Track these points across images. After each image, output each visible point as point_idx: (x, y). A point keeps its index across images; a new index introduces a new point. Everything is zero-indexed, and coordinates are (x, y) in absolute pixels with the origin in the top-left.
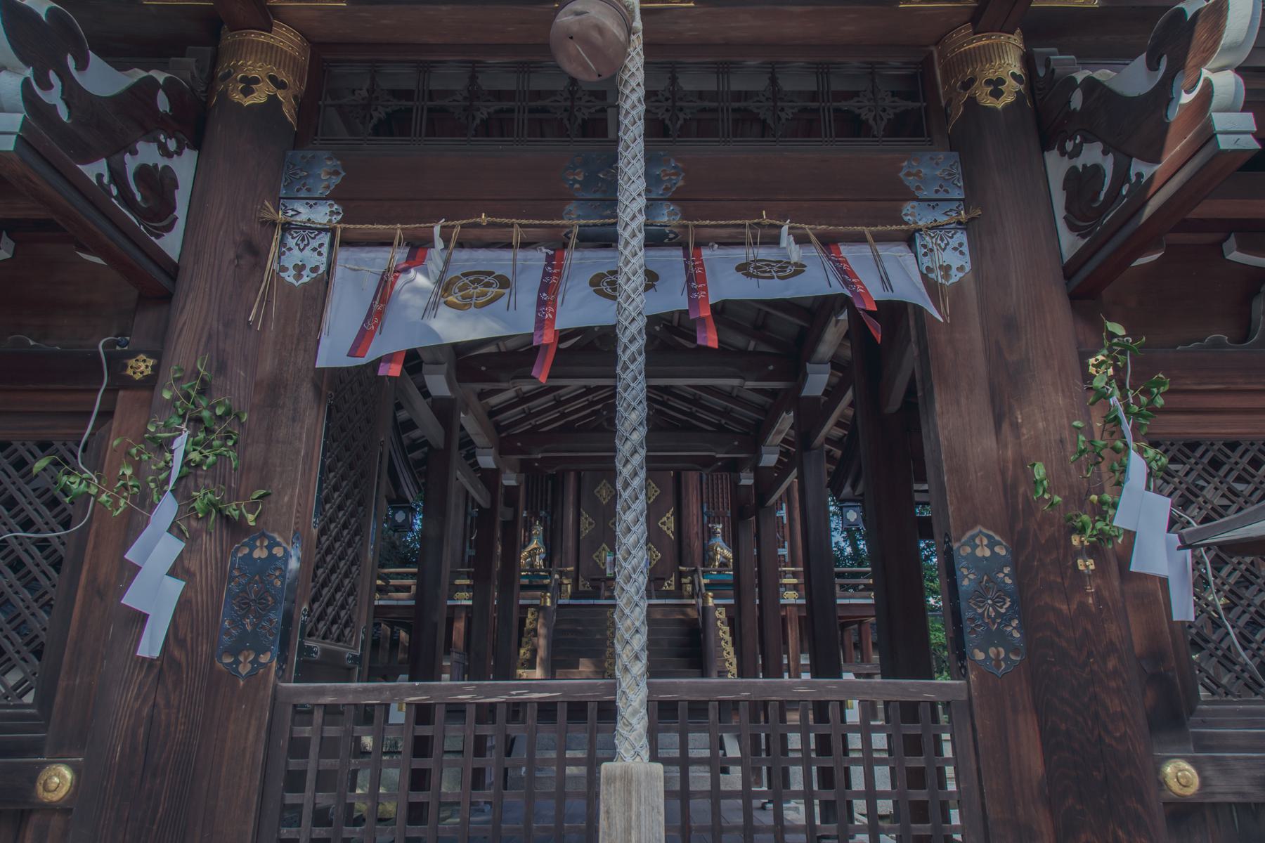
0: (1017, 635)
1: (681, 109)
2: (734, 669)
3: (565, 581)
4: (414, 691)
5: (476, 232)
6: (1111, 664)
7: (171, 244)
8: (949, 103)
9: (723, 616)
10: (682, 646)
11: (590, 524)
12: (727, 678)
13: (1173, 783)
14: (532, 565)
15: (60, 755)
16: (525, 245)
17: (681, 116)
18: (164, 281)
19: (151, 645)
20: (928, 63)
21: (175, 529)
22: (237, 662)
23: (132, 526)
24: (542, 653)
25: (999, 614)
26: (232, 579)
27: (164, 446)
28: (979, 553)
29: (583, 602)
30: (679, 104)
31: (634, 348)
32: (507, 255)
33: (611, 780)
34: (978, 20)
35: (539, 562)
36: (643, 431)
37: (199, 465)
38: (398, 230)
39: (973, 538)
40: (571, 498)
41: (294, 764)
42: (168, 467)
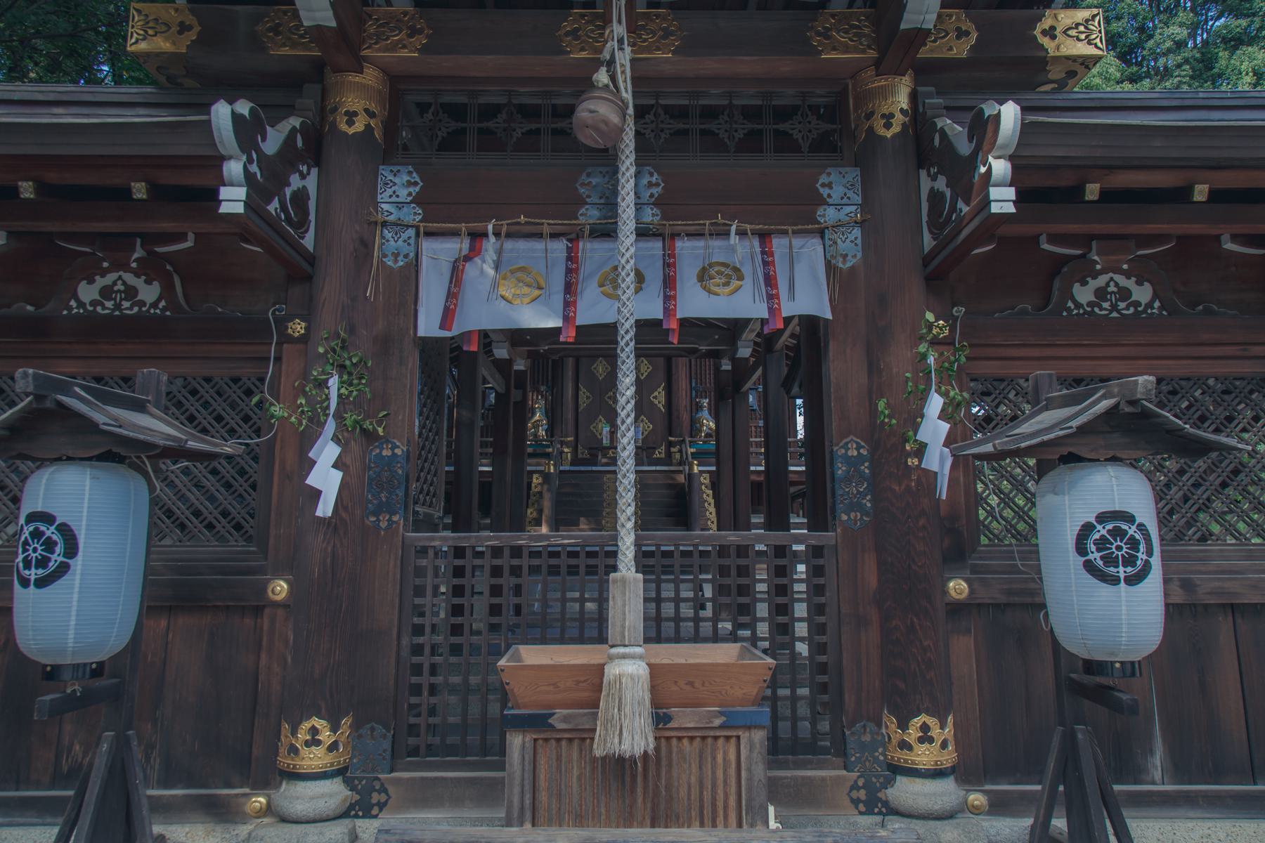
0: (869, 505)
1: (662, 130)
2: (714, 527)
3: (566, 450)
4: (490, 538)
5: (517, 227)
6: (922, 522)
7: (309, 241)
8: (857, 126)
9: (707, 481)
10: (669, 506)
11: (588, 398)
12: (709, 529)
13: (953, 593)
14: (535, 435)
15: (278, 574)
16: (554, 236)
17: (663, 135)
18: (309, 269)
19: (325, 508)
20: (843, 94)
21: (336, 439)
22: (379, 520)
23: (308, 439)
24: (547, 512)
25: (859, 492)
26: (370, 468)
27: (322, 385)
28: (850, 453)
29: (582, 468)
30: (661, 126)
31: (627, 337)
32: (538, 245)
33: (615, 581)
34: (880, 67)
35: (542, 432)
36: (633, 389)
37: (348, 397)
38: (463, 227)
39: (847, 444)
40: (569, 374)
41: (418, 581)
42: (328, 398)
